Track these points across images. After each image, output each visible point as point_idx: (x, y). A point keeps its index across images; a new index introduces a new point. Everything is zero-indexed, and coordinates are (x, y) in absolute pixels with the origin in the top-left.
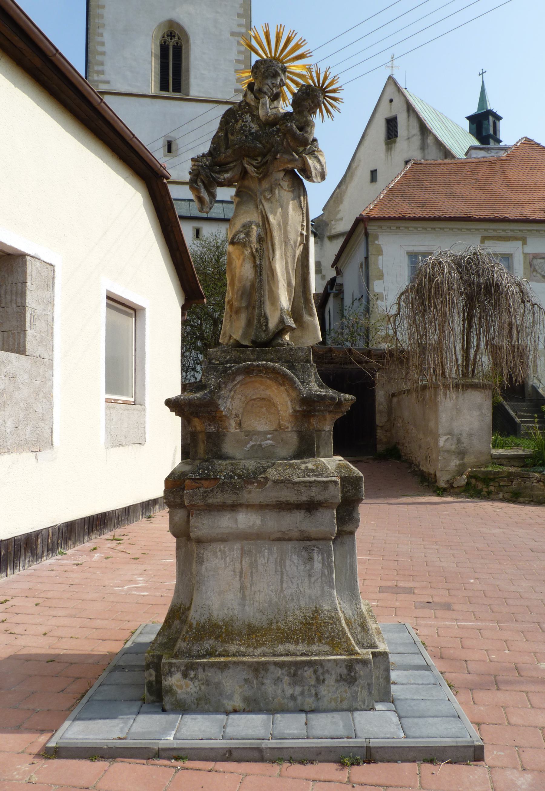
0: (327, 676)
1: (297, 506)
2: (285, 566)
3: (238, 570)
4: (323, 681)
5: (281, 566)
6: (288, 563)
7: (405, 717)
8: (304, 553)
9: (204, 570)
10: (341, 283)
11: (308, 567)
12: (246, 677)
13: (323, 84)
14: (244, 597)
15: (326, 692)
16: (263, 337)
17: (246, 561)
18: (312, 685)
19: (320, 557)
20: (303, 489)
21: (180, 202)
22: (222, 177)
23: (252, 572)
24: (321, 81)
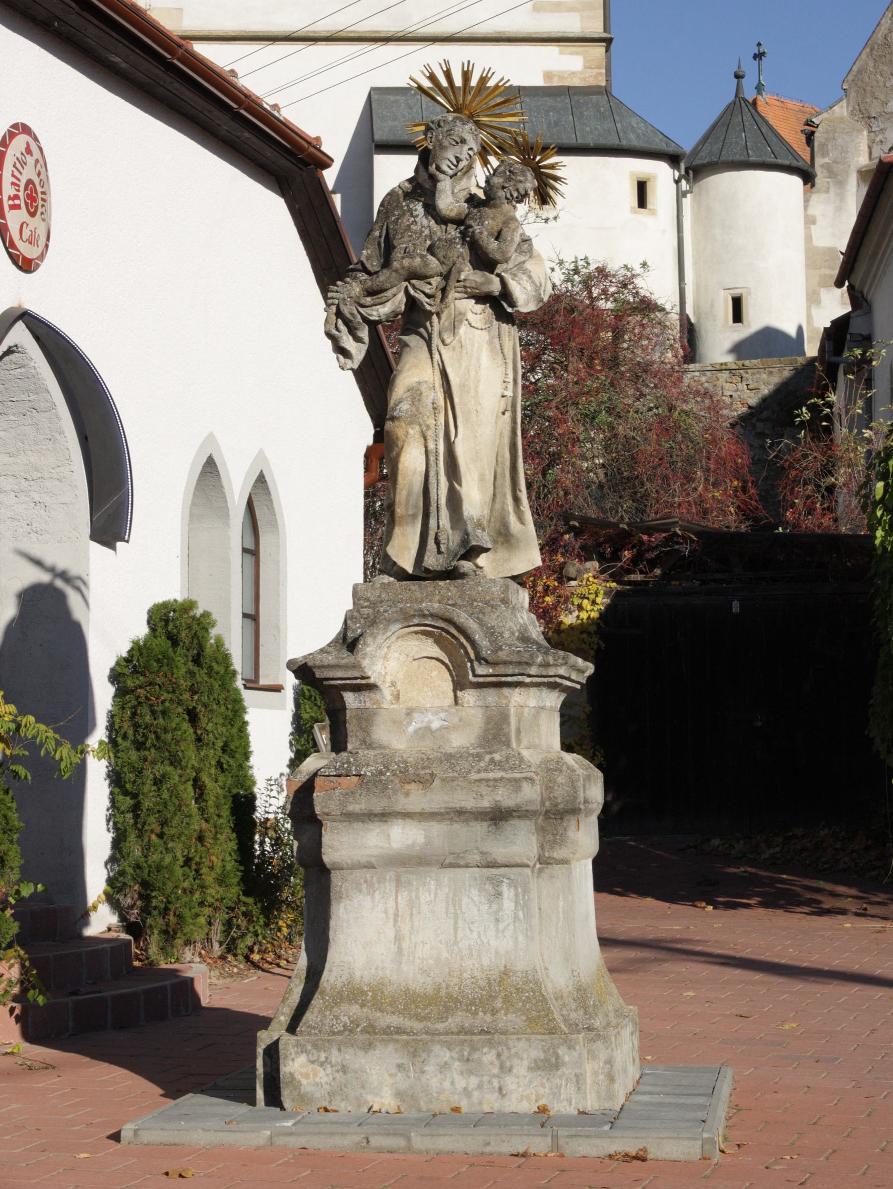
0: (515, 1061)
1: (480, 815)
3: (391, 911)
5: (454, 906)
6: (465, 900)
8: (489, 887)
11: (495, 907)
12: (399, 1061)
14: (400, 950)
15: (514, 1086)
18: (495, 1076)
19: (512, 893)
20: (484, 789)
21: (392, 98)
22: (374, 313)
23: (411, 914)
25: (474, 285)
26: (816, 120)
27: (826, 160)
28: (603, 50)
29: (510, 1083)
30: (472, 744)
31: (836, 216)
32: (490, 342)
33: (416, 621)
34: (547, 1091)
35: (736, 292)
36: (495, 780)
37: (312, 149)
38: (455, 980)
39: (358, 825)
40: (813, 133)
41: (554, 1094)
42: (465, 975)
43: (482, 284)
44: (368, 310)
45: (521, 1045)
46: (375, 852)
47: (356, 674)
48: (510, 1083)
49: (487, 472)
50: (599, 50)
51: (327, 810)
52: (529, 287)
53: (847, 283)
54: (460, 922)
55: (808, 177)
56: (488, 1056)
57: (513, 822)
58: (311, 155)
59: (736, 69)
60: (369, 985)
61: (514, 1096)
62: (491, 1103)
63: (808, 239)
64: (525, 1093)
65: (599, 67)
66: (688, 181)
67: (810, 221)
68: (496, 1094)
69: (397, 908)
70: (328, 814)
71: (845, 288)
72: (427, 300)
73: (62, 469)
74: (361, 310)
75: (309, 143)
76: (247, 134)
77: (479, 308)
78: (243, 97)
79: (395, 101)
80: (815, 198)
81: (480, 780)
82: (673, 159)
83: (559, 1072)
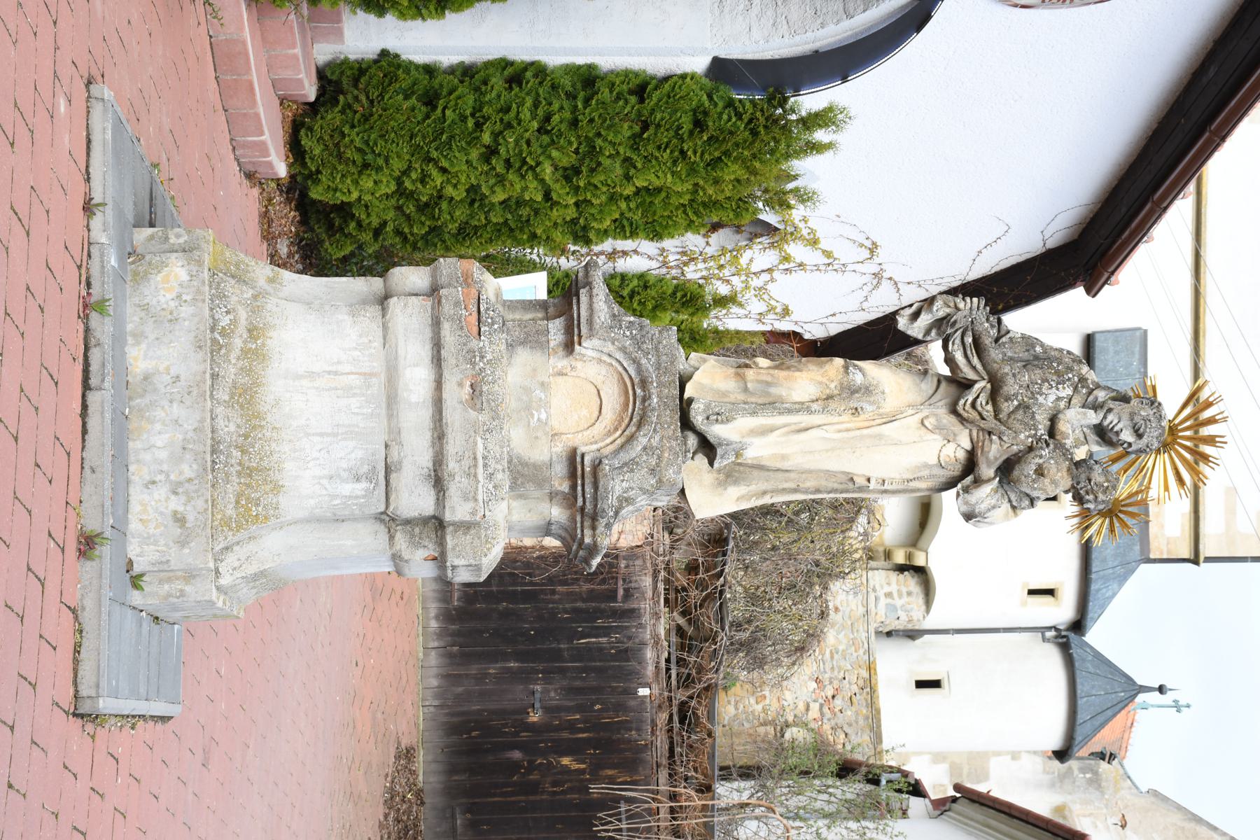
0: (183, 498)
1: (439, 461)
2: (345, 439)
3: (340, 368)
4: (175, 493)
5: (346, 433)
6: (351, 444)
7: (385, 327)
8: (365, 468)
9: (340, 317)
10: (910, 812)
11: (345, 475)
12: (182, 378)
13: (1125, 513)
14: (298, 377)
15: (156, 496)
16: (698, 419)
17: (354, 380)
18: (168, 476)
19: (359, 493)
20: (467, 463)
21: (1137, 349)
23: (337, 389)
24: (1130, 509)
25: (986, 449)
26: (1115, 762)
27: (1076, 772)
28: (1186, 556)
29: (161, 492)
30: (512, 450)
31: (1029, 787)
32: (926, 466)
33: (639, 391)
34: (151, 531)
35: (945, 683)
36: (475, 476)
37: (1106, 275)
38: (268, 434)
39: (428, 333)
40: (1103, 759)
41: (149, 538)
42: (274, 445)
43: (987, 458)
44: (958, 341)
45: (200, 504)
46: (401, 352)
47: (584, 330)
48: (161, 492)
49: (790, 463)
50: (1186, 553)
51: (444, 301)
52: (983, 507)
53: (958, 795)
54: (329, 439)
55: (1061, 755)
56: (188, 470)
57: (433, 492)
58: (1100, 275)
59: (1169, 686)
60: (263, 345)
61: (146, 497)
62: (138, 473)
63: (998, 754)
64: (149, 508)
65: (1168, 552)
66: (1056, 637)
67: (1015, 756)
68: (148, 478)
69: (342, 374)
70: (439, 302)
71: (953, 793)
72: (969, 402)
73: (785, 27)
74: (959, 332)
75: (1113, 273)
76: (1124, 210)
77: (961, 455)
78: (1165, 205)
79: (1133, 353)
80: (1039, 760)
81: (475, 458)
82: (1078, 626)
83: (171, 544)
